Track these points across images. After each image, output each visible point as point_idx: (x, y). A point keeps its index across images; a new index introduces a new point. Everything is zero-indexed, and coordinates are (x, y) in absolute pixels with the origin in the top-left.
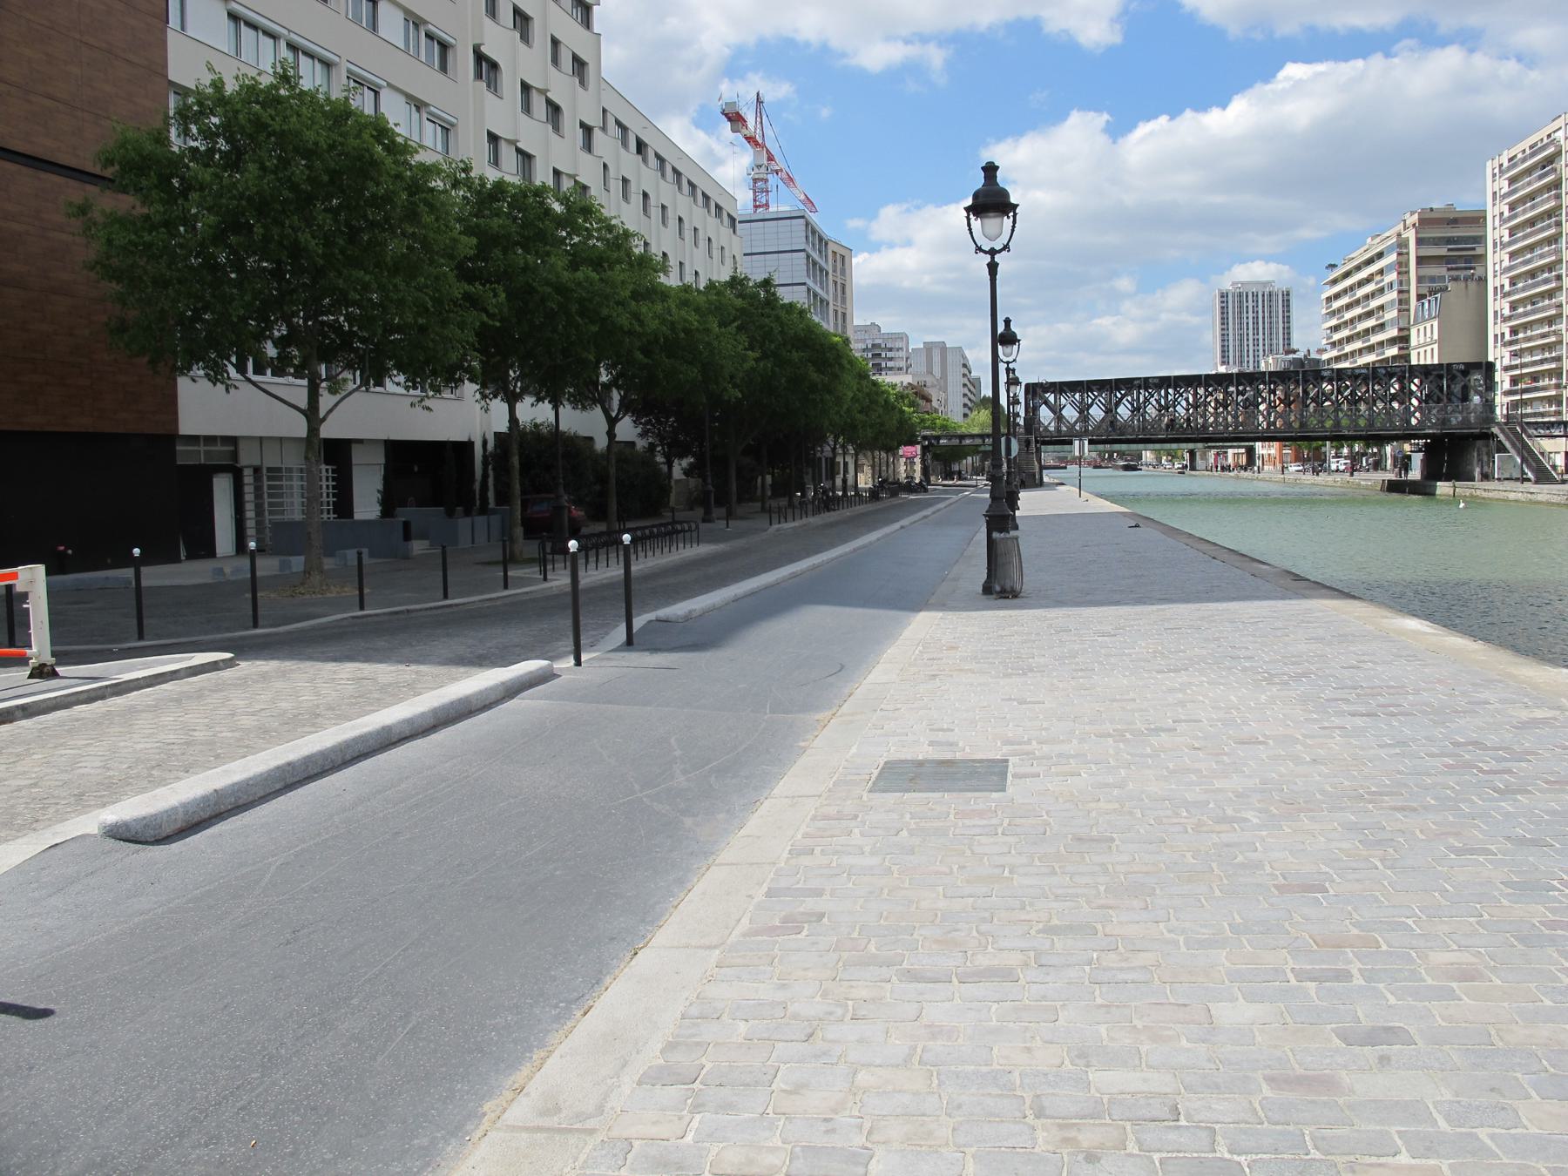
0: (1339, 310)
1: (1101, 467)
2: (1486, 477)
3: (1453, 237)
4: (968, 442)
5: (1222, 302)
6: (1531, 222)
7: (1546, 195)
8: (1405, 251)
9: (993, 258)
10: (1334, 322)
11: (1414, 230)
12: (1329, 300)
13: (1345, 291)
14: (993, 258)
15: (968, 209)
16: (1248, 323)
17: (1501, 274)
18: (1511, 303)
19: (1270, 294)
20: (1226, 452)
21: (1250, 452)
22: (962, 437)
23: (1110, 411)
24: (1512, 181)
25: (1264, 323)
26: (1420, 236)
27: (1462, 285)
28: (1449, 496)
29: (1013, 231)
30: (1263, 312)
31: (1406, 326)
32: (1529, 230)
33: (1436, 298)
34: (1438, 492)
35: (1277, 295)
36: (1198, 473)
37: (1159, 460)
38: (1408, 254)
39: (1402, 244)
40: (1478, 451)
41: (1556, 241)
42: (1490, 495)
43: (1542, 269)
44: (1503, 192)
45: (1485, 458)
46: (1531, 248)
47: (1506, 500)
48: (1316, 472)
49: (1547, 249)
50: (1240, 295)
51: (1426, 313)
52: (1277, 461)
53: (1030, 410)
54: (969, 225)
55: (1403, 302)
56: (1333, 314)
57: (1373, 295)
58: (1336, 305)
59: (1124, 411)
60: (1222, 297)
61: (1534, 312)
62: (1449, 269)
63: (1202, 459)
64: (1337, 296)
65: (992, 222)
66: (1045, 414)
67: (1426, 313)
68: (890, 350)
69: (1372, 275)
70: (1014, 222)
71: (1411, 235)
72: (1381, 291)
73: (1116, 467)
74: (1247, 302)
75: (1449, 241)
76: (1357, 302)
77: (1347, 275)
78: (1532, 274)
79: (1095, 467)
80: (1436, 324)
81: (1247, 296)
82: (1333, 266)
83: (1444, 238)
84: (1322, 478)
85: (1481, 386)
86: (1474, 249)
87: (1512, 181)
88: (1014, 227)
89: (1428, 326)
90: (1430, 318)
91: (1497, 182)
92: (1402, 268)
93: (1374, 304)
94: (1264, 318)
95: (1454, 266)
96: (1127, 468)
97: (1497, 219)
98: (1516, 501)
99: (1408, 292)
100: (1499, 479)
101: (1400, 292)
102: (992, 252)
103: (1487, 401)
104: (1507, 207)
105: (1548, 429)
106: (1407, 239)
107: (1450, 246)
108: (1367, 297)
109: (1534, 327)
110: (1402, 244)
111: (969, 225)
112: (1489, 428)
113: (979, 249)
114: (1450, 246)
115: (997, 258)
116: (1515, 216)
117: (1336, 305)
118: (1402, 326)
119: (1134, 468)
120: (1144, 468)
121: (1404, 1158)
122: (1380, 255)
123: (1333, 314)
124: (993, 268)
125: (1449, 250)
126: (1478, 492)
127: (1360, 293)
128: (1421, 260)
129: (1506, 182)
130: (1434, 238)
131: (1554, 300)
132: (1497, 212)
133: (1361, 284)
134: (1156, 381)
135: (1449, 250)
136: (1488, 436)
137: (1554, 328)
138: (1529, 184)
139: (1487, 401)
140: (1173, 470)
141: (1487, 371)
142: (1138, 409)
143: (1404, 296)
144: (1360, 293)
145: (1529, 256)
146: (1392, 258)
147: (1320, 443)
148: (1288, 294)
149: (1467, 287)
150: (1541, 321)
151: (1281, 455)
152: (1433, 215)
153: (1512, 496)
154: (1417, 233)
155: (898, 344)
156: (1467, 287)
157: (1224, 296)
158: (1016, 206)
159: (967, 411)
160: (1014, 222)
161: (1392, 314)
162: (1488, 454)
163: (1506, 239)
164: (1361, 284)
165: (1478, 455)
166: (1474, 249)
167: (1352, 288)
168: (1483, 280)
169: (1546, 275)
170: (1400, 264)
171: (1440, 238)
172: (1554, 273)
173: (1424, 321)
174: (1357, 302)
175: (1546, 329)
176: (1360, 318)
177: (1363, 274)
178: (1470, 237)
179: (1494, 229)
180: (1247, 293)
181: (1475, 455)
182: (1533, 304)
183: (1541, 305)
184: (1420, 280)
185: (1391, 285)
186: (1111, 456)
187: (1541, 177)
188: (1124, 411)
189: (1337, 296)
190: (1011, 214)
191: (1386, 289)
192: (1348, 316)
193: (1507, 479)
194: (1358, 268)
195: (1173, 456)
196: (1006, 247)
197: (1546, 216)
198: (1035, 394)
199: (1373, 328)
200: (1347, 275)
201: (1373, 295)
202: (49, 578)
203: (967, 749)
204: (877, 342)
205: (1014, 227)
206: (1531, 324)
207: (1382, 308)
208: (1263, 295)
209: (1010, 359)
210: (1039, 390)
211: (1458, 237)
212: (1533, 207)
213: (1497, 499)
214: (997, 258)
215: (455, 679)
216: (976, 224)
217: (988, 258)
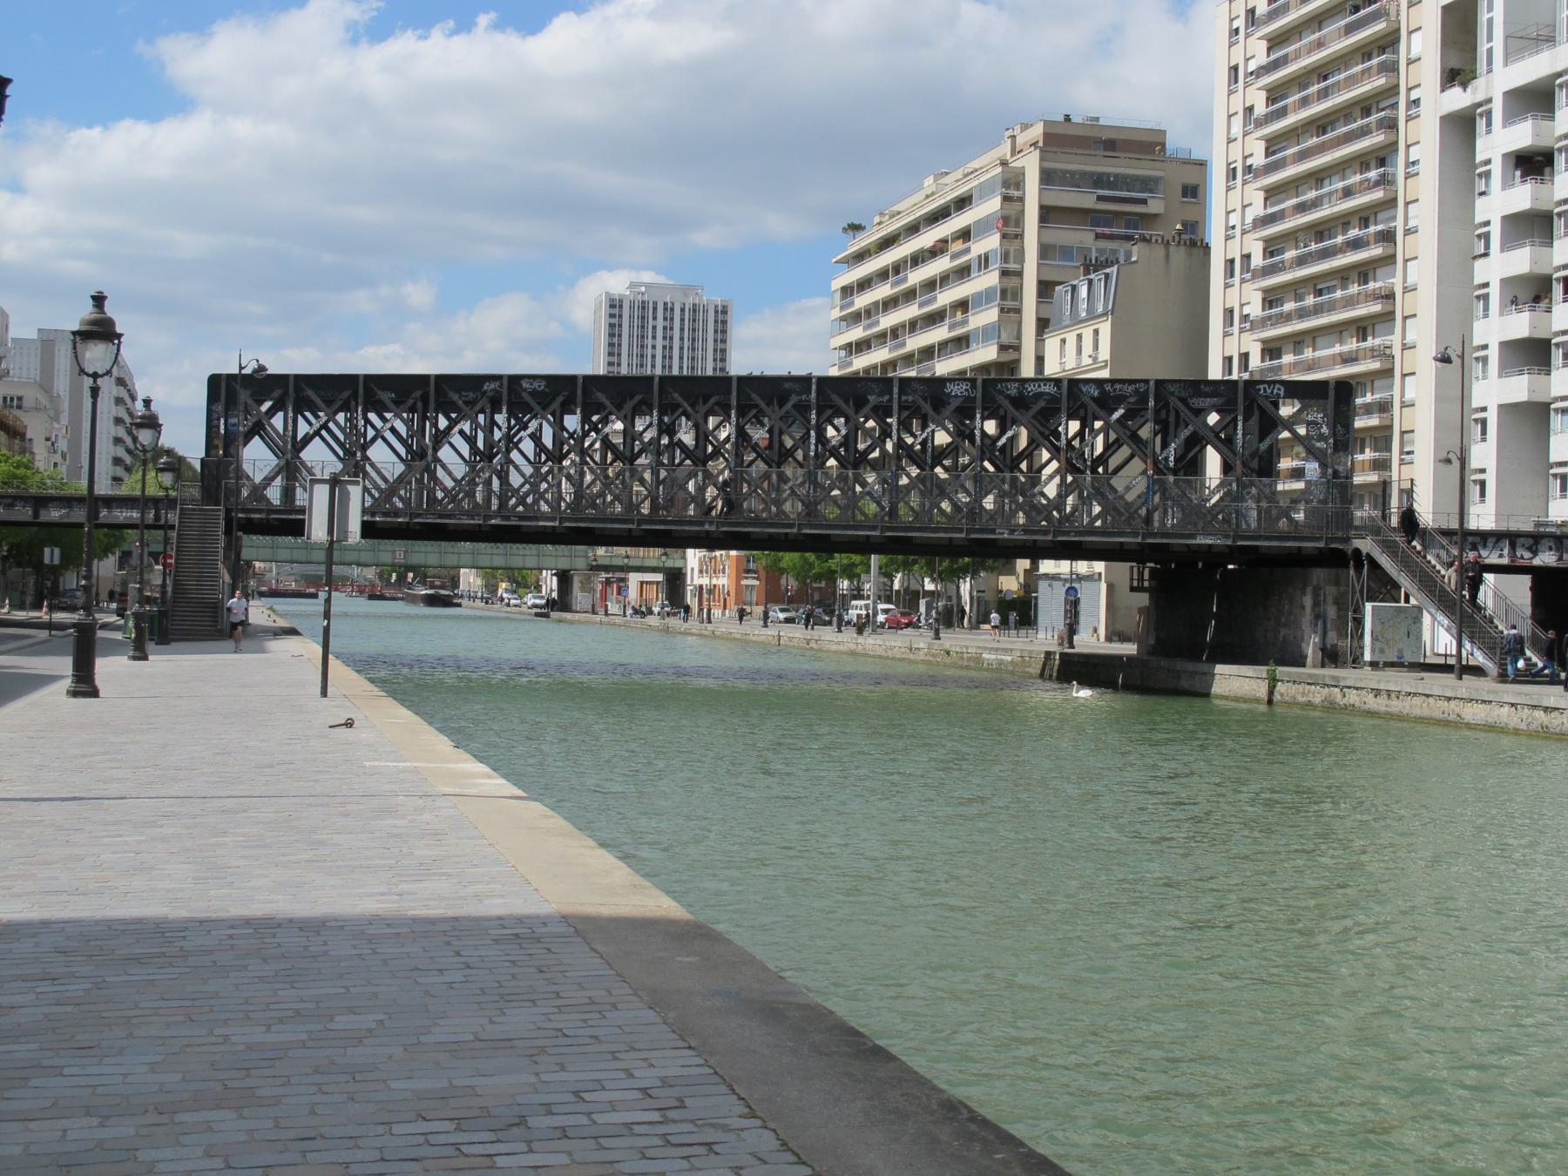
0: (869, 312)
1: (382, 597)
2: (1331, 657)
3: (1108, 175)
4: (55, 514)
5: (612, 316)
6: (1320, 125)
7: (1360, 68)
8: (1016, 193)
9: (95, 382)
10: (857, 333)
11: (1036, 154)
12: (847, 291)
13: (883, 275)
16: (654, 356)
17: (1244, 233)
18: (1266, 291)
19: (694, 310)
20: (624, 580)
21: (675, 580)
22: (41, 502)
23: (420, 457)
24: (1275, 42)
25: (681, 358)
26: (1049, 165)
27: (1159, 251)
28: (1257, 701)
30: (682, 339)
31: (1014, 341)
32: (1314, 140)
33: (1107, 276)
34: (1217, 688)
35: (706, 311)
36: (577, 616)
37: (491, 588)
38: (1021, 199)
39: (1012, 183)
40: (1316, 596)
41: (1382, 162)
42: (1396, 706)
43: (1344, 221)
44: (1252, 66)
45: (1332, 612)
46: (1317, 177)
47: (1458, 724)
48: (810, 620)
49: (1357, 178)
50: (644, 306)
51: (1083, 306)
52: (731, 600)
53: (219, 442)
55: (1009, 297)
56: (855, 318)
57: (944, 280)
58: (862, 301)
59: (453, 459)
60: (612, 306)
61: (1317, 310)
62: (1098, 236)
63: (583, 589)
64: (864, 285)
66: (257, 458)
67: (1083, 306)
69: (944, 241)
71: (1031, 165)
72: (963, 272)
73: (413, 599)
74: (655, 318)
75: (1099, 181)
76: (910, 295)
77: (887, 243)
78: (1320, 231)
79: (372, 597)
80: (1105, 328)
81: (655, 309)
82: (856, 228)
83: (1092, 174)
84: (827, 635)
85: (1321, 437)
86: (1144, 202)
87: (1275, 42)
89: (1087, 334)
90: (1092, 316)
91: (1240, 46)
92: (1010, 225)
93: (945, 298)
94: (681, 349)
95: (1107, 230)
96: (432, 601)
97: (1240, 118)
98: (1491, 728)
99: (1020, 274)
100: (1374, 665)
101: (1004, 273)
102: (95, 376)
103: (1336, 474)
104: (1263, 94)
105: (1474, 547)
106: (1021, 173)
107: (1101, 192)
108: (931, 285)
109: (1319, 341)
110: (1012, 183)
112: (1347, 540)
114: (1101, 192)
116: (1282, 113)
117: (862, 301)
118: (1005, 339)
119: (446, 602)
120: (465, 602)
122: (963, 203)
123: (855, 318)
125: (1100, 198)
126: (1353, 697)
127: (916, 277)
129: (1264, 45)
130: (1073, 173)
131: (1371, 285)
132: (1237, 105)
133: (917, 259)
134: (540, 386)
135: (1100, 198)
136: (1339, 559)
137: (1370, 342)
138: (1320, 44)
139: (1336, 474)
140: (524, 609)
141: (1338, 402)
142: (488, 456)
143: (1012, 282)
144: (916, 277)
145: (1312, 194)
146: (991, 206)
147: (856, 558)
148: (725, 312)
149: (1167, 256)
150: (1339, 330)
152: (1069, 131)
153: (1475, 713)
154: (1042, 159)
156: (1167, 256)
157: (615, 305)
159: (120, 472)
161: (986, 316)
162: (1340, 602)
163: (1259, 160)
164: (917, 259)
165: (1316, 604)
166: (1144, 202)
167: (898, 268)
168: (1198, 248)
169: (1354, 233)
170: (1006, 220)
171: (1084, 174)
172: (1372, 229)
173: (1077, 321)
174: (910, 295)
175: (1351, 345)
176: (913, 326)
177: (927, 238)
178: (1136, 178)
179: (1230, 141)
180: (655, 303)
181: (1308, 601)
182: (1319, 293)
183: (1339, 294)
184: (1045, 251)
185: (984, 261)
186: (402, 578)
187: (1350, 29)
188: (453, 459)
189: (864, 285)
191: (974, 267)
192: (887, 321)
193: (1392, 665)
194: (913, 229)
195: (522, 582)
197: (1357, 112)
198: (231, 404)
199: (943, 345)
200: (887, 243)
201: (944, 280)
206: (1312, 336)
207: (963, 305)
208: (683, 310)
210: (244, 396)
211: (1116, 176)
212: (1324, 94)
213: (1421, 720)
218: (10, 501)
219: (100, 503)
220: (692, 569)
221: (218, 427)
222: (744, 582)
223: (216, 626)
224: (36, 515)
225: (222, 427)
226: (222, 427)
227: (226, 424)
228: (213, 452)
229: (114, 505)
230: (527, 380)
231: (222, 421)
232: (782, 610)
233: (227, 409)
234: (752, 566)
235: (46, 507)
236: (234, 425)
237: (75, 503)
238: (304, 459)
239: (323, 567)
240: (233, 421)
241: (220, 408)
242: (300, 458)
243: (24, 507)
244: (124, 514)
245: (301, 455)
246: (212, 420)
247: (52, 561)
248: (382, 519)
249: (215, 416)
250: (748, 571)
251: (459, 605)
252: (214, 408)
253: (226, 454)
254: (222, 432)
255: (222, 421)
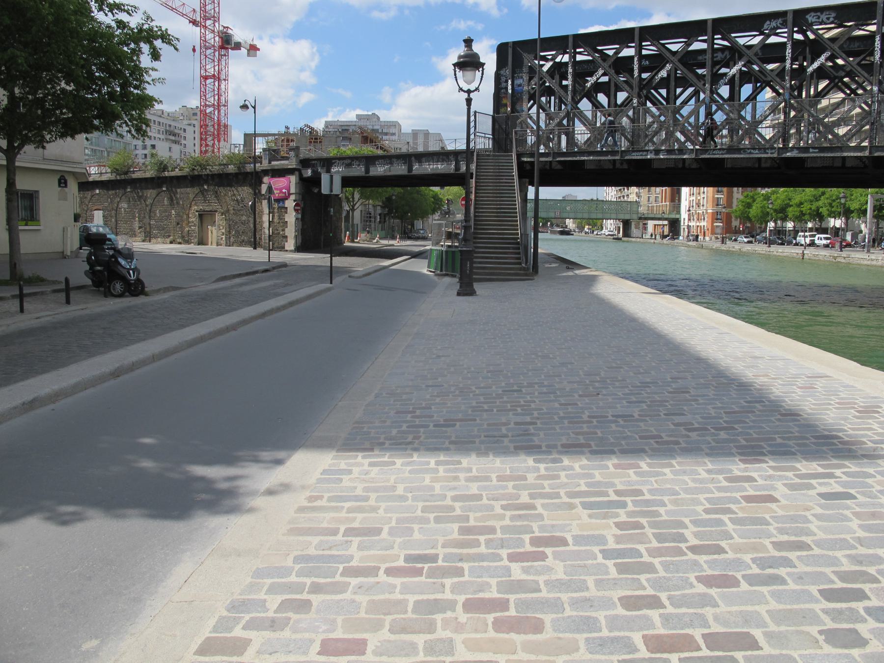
9: (469, 95)
14: (469, 95)
15: (454, 65)
29: (481, 79)
36: (633, 240)
53: (507, 101)
54: (455, 74)
65: (469, 74)
68: (386, 134)
70: (483, 74)
73: (553, 232)
88: (482, 77)
102: (469, 92)
111: (455, 74)
113: (461, 89)
115: (472, 95)
121: (705, 652)
124: (469, 101)
128: (516, 213)
151: (713, 228)
155: (392, 130)
158: (484, 64)
160: (483, 74)
190: (481, 69)
196: (477, 89)
202: (677, 216)
203: (432, 464)
204: (375, 127)
205: (482, 77)
209: (472, 87)
214: (472, 95)
215: (379, 261)
216: (460, 74)
217: (466, 95)
218: (349, 161)
219: (413, 159)
220: (684, 219)
221: (506, 88)
222: (715, 224)
223: (520, 264)
224: (367, 171)
225: (510, 87)
226: (510, 87)
227: (513, 84)
228: (502, 110)
229: (424, 159)
230: (813, 14)
231: (510, 82)
232: (745, 237)
233: (513, 72)
234: (719, 217)
235: (374, 164)
236: (520, 85)
237: (395, 160)
238: (582, 109)
239: (25, 292)
240: (517, 82)
241: (507, 72)
242: (579, 109)
243: (359, 165)
244: (431, 166)
245: (579, 106)
246: (500, 84)
247: (331, 190)
248: (666, 157)
249: (503, 79)
250: (717, 219)
251: (573, 235)
252: (502, 72)
253: (513, 111)
254: (510, 91)
255: (510, 82)
